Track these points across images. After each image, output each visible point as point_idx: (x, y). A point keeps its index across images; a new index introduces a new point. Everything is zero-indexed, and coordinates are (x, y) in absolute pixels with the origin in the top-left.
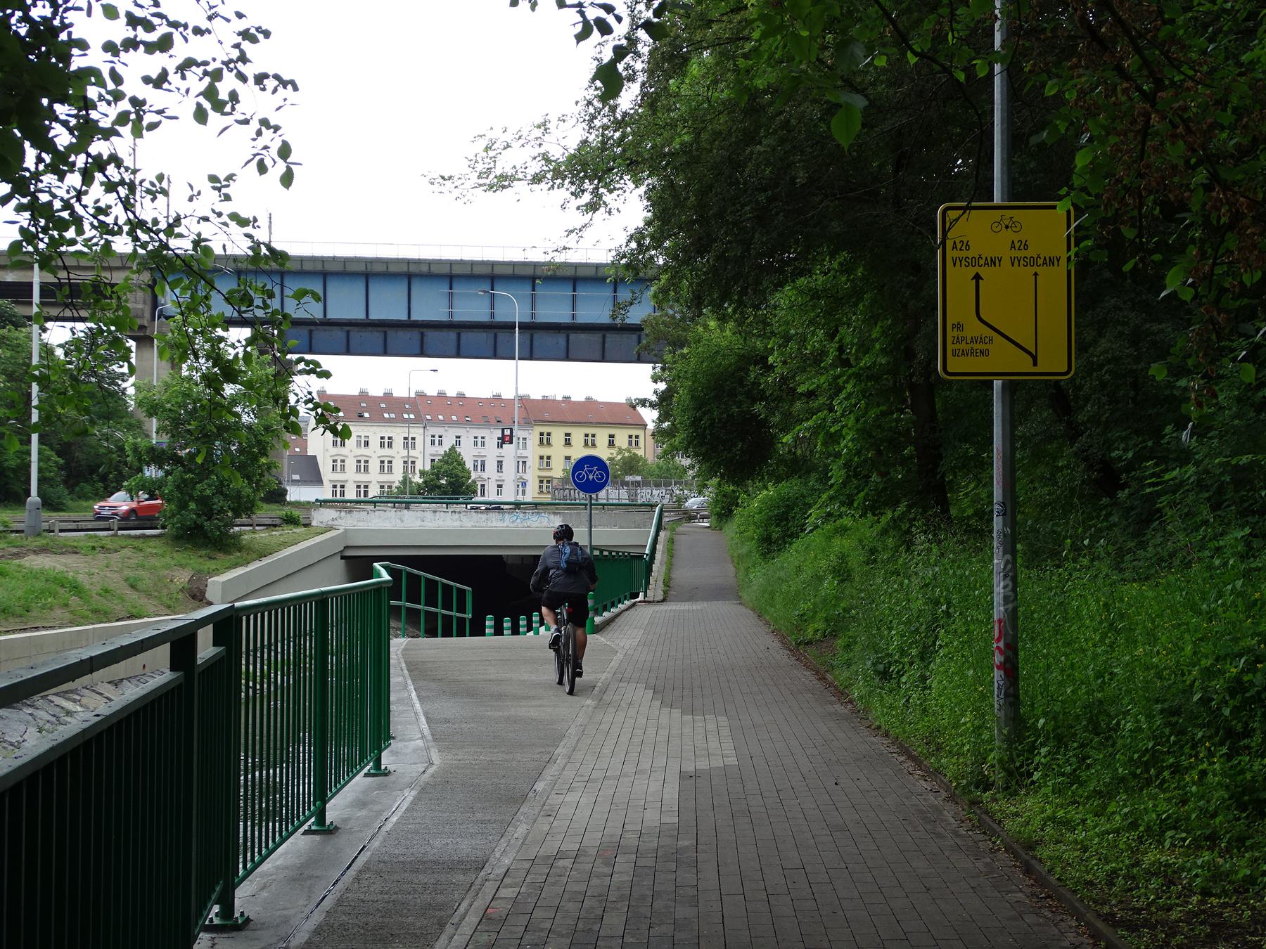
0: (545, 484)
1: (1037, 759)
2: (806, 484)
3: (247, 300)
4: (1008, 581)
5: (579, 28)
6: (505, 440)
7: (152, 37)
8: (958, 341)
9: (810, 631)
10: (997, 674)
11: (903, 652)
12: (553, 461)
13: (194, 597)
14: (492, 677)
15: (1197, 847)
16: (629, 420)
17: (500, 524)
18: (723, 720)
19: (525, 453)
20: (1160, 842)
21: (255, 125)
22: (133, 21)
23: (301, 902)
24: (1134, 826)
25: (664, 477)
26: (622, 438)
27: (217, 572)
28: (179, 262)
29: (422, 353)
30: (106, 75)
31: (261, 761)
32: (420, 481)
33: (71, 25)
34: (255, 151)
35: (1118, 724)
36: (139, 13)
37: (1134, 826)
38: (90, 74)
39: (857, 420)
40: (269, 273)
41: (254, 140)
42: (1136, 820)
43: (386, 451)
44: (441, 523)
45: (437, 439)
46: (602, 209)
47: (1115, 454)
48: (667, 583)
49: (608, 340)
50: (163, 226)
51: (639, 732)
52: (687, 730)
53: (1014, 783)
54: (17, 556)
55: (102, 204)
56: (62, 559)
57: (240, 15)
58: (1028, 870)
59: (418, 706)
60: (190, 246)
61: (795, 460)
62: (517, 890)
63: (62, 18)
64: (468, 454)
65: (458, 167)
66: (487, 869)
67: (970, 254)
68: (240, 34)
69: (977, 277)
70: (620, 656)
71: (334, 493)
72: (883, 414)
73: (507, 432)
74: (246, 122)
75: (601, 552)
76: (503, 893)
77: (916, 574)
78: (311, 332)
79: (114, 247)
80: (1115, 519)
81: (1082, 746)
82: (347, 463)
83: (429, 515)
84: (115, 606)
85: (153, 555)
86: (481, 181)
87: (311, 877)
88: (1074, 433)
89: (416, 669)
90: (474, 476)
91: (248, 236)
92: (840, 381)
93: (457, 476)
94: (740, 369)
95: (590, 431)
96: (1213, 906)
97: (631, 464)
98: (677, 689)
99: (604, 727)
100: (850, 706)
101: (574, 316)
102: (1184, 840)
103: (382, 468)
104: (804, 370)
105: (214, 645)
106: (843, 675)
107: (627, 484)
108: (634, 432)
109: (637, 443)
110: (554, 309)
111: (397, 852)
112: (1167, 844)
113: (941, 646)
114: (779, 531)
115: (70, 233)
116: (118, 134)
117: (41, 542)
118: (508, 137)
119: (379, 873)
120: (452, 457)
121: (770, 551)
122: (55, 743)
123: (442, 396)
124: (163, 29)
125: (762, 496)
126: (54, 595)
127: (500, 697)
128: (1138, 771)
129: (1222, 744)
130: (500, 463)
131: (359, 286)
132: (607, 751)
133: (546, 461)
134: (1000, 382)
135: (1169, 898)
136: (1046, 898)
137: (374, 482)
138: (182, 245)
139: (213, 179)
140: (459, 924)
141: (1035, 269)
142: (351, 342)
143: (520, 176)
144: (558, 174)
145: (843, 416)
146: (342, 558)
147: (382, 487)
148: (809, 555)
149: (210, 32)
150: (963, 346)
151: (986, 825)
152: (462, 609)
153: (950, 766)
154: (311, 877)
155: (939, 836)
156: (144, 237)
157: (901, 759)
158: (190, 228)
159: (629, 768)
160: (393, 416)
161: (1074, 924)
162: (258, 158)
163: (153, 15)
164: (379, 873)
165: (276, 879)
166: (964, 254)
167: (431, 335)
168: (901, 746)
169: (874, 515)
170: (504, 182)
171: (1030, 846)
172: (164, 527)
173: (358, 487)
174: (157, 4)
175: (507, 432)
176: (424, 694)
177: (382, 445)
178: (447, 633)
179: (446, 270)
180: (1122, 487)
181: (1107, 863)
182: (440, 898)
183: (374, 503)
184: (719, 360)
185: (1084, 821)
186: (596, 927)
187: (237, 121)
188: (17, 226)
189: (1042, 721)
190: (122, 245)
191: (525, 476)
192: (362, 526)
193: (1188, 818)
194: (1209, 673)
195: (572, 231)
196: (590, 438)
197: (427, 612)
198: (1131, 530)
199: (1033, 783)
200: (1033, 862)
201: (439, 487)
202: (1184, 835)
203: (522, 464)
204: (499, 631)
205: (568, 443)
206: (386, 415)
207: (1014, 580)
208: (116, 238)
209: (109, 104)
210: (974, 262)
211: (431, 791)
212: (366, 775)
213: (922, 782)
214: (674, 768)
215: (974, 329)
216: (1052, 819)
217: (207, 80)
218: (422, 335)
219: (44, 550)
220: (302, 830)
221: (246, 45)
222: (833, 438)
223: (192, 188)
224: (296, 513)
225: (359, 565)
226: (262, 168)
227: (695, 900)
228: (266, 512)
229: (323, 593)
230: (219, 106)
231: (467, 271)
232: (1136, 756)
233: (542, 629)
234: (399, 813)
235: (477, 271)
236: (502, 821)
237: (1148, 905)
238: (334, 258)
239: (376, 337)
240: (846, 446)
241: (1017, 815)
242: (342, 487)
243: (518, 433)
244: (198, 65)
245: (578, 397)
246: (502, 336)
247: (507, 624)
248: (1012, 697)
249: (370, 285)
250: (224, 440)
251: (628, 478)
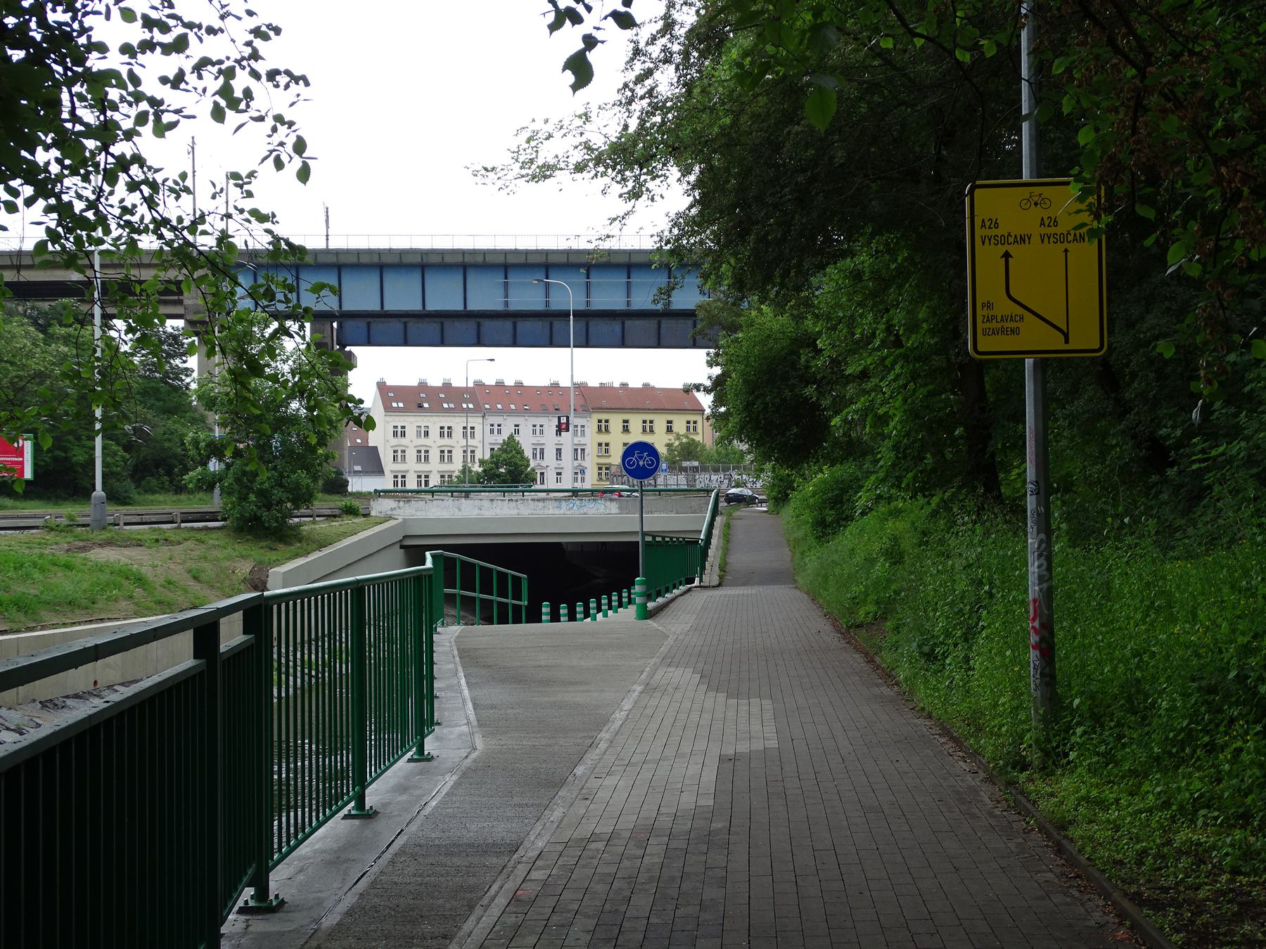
0: (604, 471)
1: (1073, 739)
2: (860, 468)
3: (270, 295)
4: (1042, 560)
5: (551, 17)
6: (562, 428)
7: (168, 38)
8: (989, 319)
9: (862, 613)
10: (1033, 655)
11: (948, 634)
12: (611, 448)
14: (542, 663)
15: (1228, 826)
16: (686, 405)
17: (557, 511)
18: (767, 704)
19: (583, 441)
20: (1193, 821)
21: (270, 122)
22: (149, 23)
23: (335, 885)
24: (1166, 805)
25: (723, 463)
26: (680, 424)
27: (278, 563)
28: (202, 258)
29: (479, 343)
30: (125, 76)
31: (324, 749)
32: (480, 470)
33: (91, 29)
34: (271, 147)
35: (1155, 702)
36: (154, 15)
37: (1166, 805)
38: (109, 76)
39: (905, 401)
40: (287, 267)
41: (270, 136)
42: (1169, 798)
44: (498, 511)
45: (496, 428)
46: (645, 197)
47: (1163, 431)
48: (723, 568)
49: (663, 326)
50: (187, 223)
51: (683, 716)
52: (731, 714)
53: (1050, 762)
54: (84, 549)
55: (128, 204)
56: (127, 552)
57: (250, 13)
58: (1060, 850)
59: (466, 692)
60: (214, 243)
61: (850, 443)
62: (548, 872)
63: (81, 23)
64: (526, 442)
65: (501, 158)
66: (521, 852)
67: (999, 232)
68: (251, 32)
69: (1007, 255)
70: (670, 641)
71: (396, 484)
72: (931, 394)
73: (564, 420)
74: (261, 119)
75: (654, 537)
76: (535, 875)
77: (960, 555)
78: (369, 324)
79: (140, 245)
80: (1164, 496)
81: (1119, 725)
82: (407, 454)
83: (486, 503)
84: (179, 597)
85: (215, 547)
86: (524, 172)
87: (346, 861)
88: (1123, 410)
89: (468, 656)
90: (532, 464)
91: (269, 231)
92: (887, 362)
93: (516, 464)
94: (792, 353)
95: (648, 417)
96: (1242, 885)
97: (689, 450)
98: (727, 672)
99: (649, 711)
100: (896, 688)
101: (628, 303)
102: (1216, 818)
103: (442, 458)
104: (854, 352)
105: (245, 633)
106: (886, 658)
107: (685, 469)
108: (692, 418)
109: (695, 429)
110: (609, 296)
111: (433, 835)
112: (1200, 823)
113: (983, 628)
114: (832, 515)
115: (99, 233)
116: (139, 134)
117: (106, 535)
118: (549, 128)
119: (414, 857)
120: (511, 446)
121: (824, 534)
122: (57, 728)
123: (500, 385)
124: (180, 30)
125: (817, 479)
126: (119, 587)
127: (548, 682)
128: (1174, 750)
129: (1256, 722)
130: (559, 451)
131: (415, 279)
132: (649, 735)
133: (605, 448)
134: (1032, 360)
135: (1198, 877)
136: (1075, 878)
137: (435, 472)
138: (206, 242)
139: (235, 176)
140: (488, 906)
141: (1066, 245)
142: (446, 335)
143: (562, 165)
144: (598, 161)
145: (891, 397)
146: (402, 547)
147: (442, 476)
148: (861, 539)
149: (222, 31)
150: (994, 325)
151: (1021, 805)
152: (517, 596)
153: (987, 745)
154: (346, 861)
155: (973, 816)
156: (169, 235)
157: (943, 740)
158: (215, 224)
159: (670, 752)
160: (452, 406)
161: (1101, 903)
162: (275, 154)
163: (169, 16)
164: (414, 857)
165: (315, 863)
166: (993, 232)
167: (487, 324)
168: (943, 728)
169: (925, 496)
170: (546, 172)
171: (1063, 826)
172: (224, 519)
173: (419, 477)
174: (171, 6)
175: (564, 420)
176: (473, 681)
177: (442, 435)
178: (503, 620)
179: (501, 260)
180: (1172, 465)
181: (1138, 842)
182: (472, 881)
183: (432, 492)
184: (771, 343)
185: (1117, 800)
186: (623, 908)
187: (252, 118)
188: (44, 226)
189: (1077, 701)
190: (148, 242)
191: (584, 464)
192: (420, 515)
193: (1221, 797)
194: (1246, 651)
195: (615, 219)
196: (648, 424)
197: (481, 599)
198: (1180, 508)
199: (1069, 763)
200: (1065, 842)
201: (499, 475)
202: (1216, 814)
203: (579, 452)
204: (555, 617)
205: (626, 430)
206: (445, 406)
207: (1049, 559)
208: (143, 237)
209: (130, 105)
210: (1002, 240)
211: (472, 776)
212: (409, 761)
213: (961, 763)
214: (715, 752)
215: (1004, 307)
216: (1086, 799)
217: (221, 80)
218: (479, 325)
219: (108, 543)
220: (341, 814)
221: (258, 43)
222: (883, 420)
223: (214, 185)
224: (356, 503)
225: (414, 553)
226: (279, 164)
227: (723, 883)
228: (324, 503)
229: (358, 581)
230: (234, 104)
231: (522, 260)
232: (1171, 735)
233: (600, 616)
234: (439, 798)
235: (531, 260)
236: (539, 805)
237: (1177, 884)
238: (390, 250)
239: (432, 328)
240: (895, 428)
241: (1052, 795)
242: (403, 477)
243: (574, 421)
244: (213, 64)
245: (635, 383)
246: (558, 324)
247: (563, 610)
248: (1048, 676)
249: (427, 277)
250: (282, 433)
251: (685, 464)
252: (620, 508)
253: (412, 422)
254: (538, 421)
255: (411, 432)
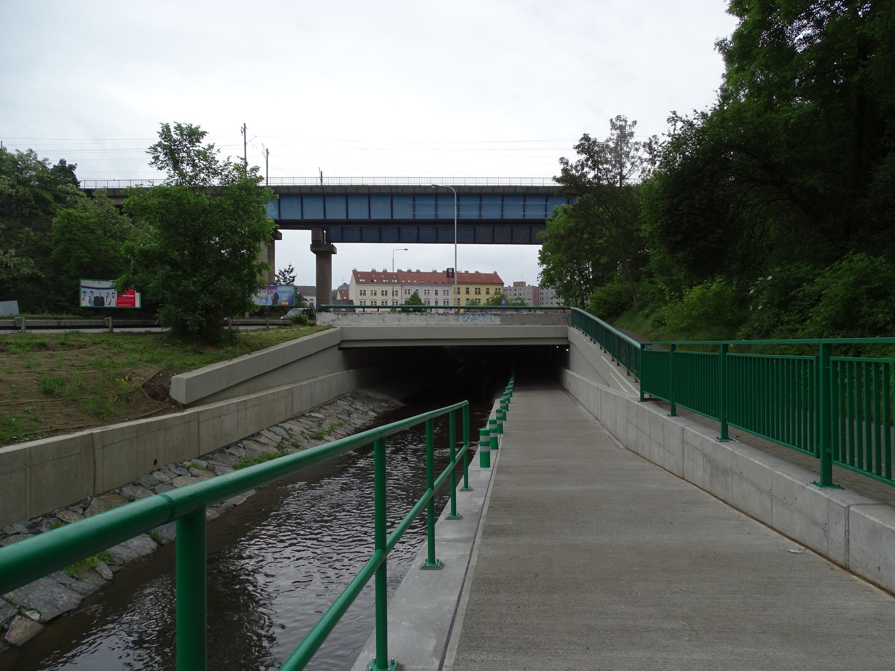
13: (155, 396)
17: (456, 323)
27: (184, 369)
29: (399, 241)
43: (384, 297)
64: (422, 297)
95: (478, 287)
108: (498, 287)
123: (409, 271)
177: (382, 294)
192: (354, 325)
205: (468, 292)
245: (472, 271)
252: (502, 321)
253: (369, 289)
254: (427, 288)
255: (368, 293)
